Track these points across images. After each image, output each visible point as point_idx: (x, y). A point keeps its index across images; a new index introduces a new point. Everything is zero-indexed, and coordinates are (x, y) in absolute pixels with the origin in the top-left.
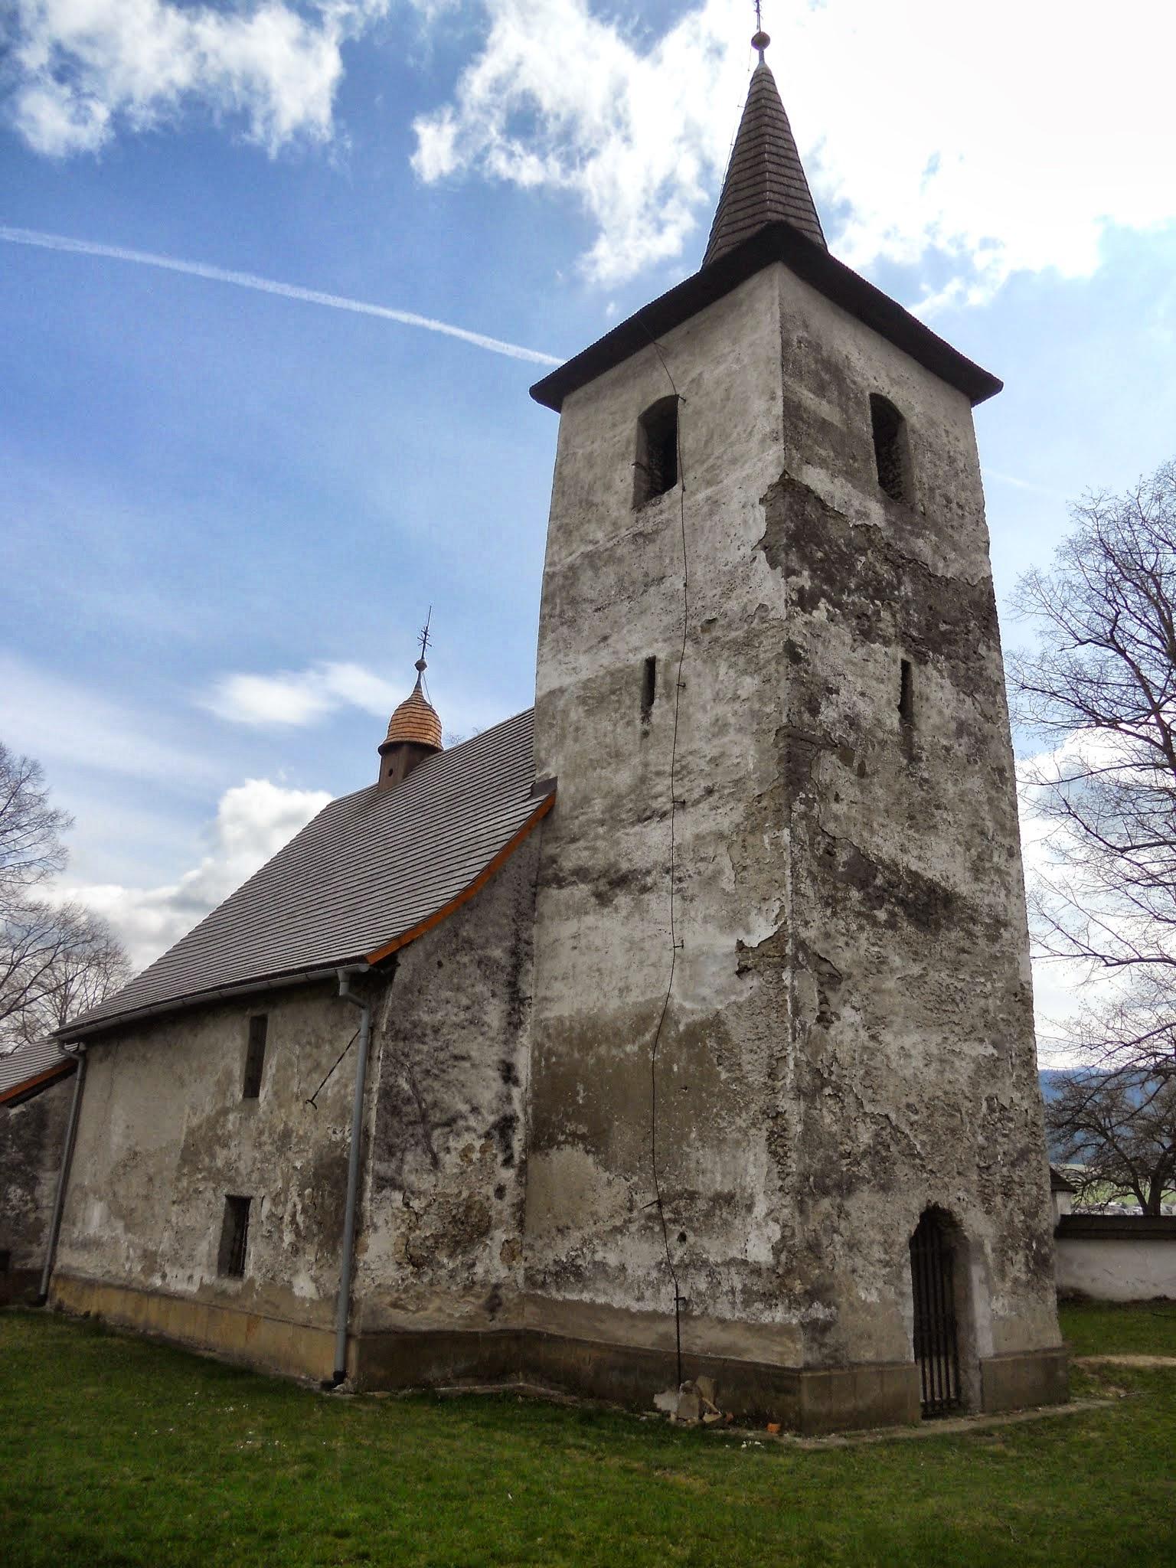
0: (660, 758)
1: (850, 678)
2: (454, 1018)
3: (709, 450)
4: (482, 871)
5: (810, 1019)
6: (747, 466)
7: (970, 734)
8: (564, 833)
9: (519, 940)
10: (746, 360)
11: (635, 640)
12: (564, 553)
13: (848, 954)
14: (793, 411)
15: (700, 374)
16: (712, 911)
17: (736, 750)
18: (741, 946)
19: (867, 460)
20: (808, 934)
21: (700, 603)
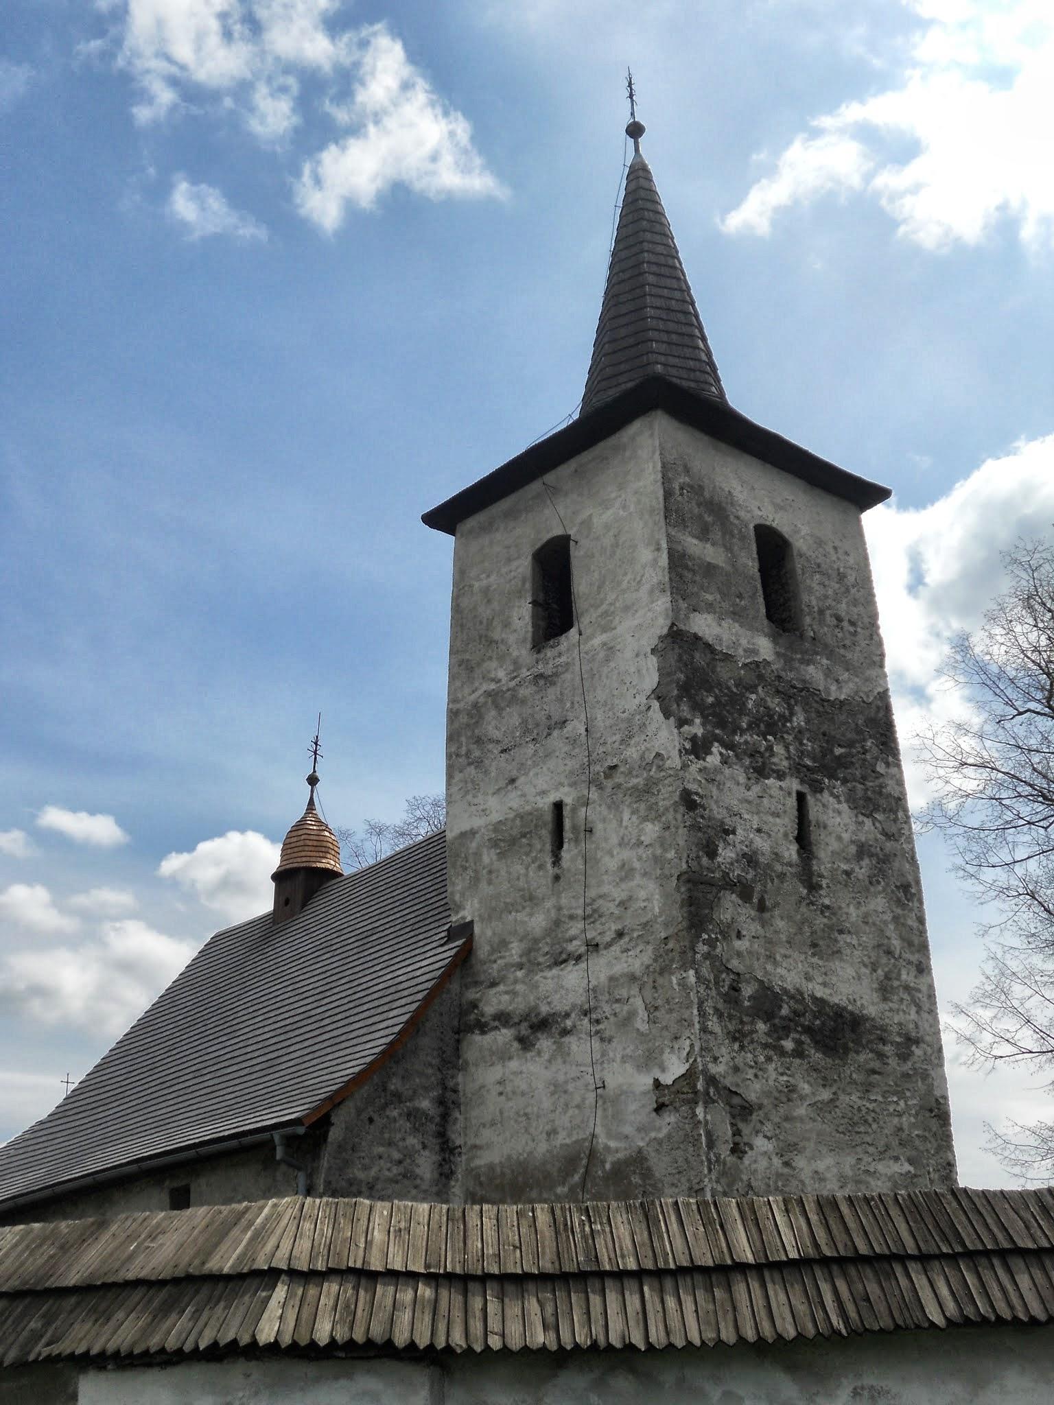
0: (571, 901)
1: (746, 816)
2: (387, 1173)
3: (602, 596)
4: (407, 1022)
5: (724, 1150)
6: (638, 615)
7: (871, 855)
8: (482, 977)
9: (445, 1088)
10: (632, 508)
11: (541, 783)
12: (467, 691)
13: (757, 1086)
14: (678, 562)
15: (590, 516)
16: (628, 1051)
17: (642, 894)
18: (657, 1084)
19: (753, 597)
20: (717, 1069)
21: (602, 749)
